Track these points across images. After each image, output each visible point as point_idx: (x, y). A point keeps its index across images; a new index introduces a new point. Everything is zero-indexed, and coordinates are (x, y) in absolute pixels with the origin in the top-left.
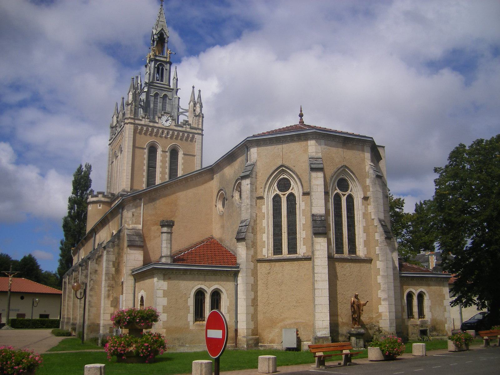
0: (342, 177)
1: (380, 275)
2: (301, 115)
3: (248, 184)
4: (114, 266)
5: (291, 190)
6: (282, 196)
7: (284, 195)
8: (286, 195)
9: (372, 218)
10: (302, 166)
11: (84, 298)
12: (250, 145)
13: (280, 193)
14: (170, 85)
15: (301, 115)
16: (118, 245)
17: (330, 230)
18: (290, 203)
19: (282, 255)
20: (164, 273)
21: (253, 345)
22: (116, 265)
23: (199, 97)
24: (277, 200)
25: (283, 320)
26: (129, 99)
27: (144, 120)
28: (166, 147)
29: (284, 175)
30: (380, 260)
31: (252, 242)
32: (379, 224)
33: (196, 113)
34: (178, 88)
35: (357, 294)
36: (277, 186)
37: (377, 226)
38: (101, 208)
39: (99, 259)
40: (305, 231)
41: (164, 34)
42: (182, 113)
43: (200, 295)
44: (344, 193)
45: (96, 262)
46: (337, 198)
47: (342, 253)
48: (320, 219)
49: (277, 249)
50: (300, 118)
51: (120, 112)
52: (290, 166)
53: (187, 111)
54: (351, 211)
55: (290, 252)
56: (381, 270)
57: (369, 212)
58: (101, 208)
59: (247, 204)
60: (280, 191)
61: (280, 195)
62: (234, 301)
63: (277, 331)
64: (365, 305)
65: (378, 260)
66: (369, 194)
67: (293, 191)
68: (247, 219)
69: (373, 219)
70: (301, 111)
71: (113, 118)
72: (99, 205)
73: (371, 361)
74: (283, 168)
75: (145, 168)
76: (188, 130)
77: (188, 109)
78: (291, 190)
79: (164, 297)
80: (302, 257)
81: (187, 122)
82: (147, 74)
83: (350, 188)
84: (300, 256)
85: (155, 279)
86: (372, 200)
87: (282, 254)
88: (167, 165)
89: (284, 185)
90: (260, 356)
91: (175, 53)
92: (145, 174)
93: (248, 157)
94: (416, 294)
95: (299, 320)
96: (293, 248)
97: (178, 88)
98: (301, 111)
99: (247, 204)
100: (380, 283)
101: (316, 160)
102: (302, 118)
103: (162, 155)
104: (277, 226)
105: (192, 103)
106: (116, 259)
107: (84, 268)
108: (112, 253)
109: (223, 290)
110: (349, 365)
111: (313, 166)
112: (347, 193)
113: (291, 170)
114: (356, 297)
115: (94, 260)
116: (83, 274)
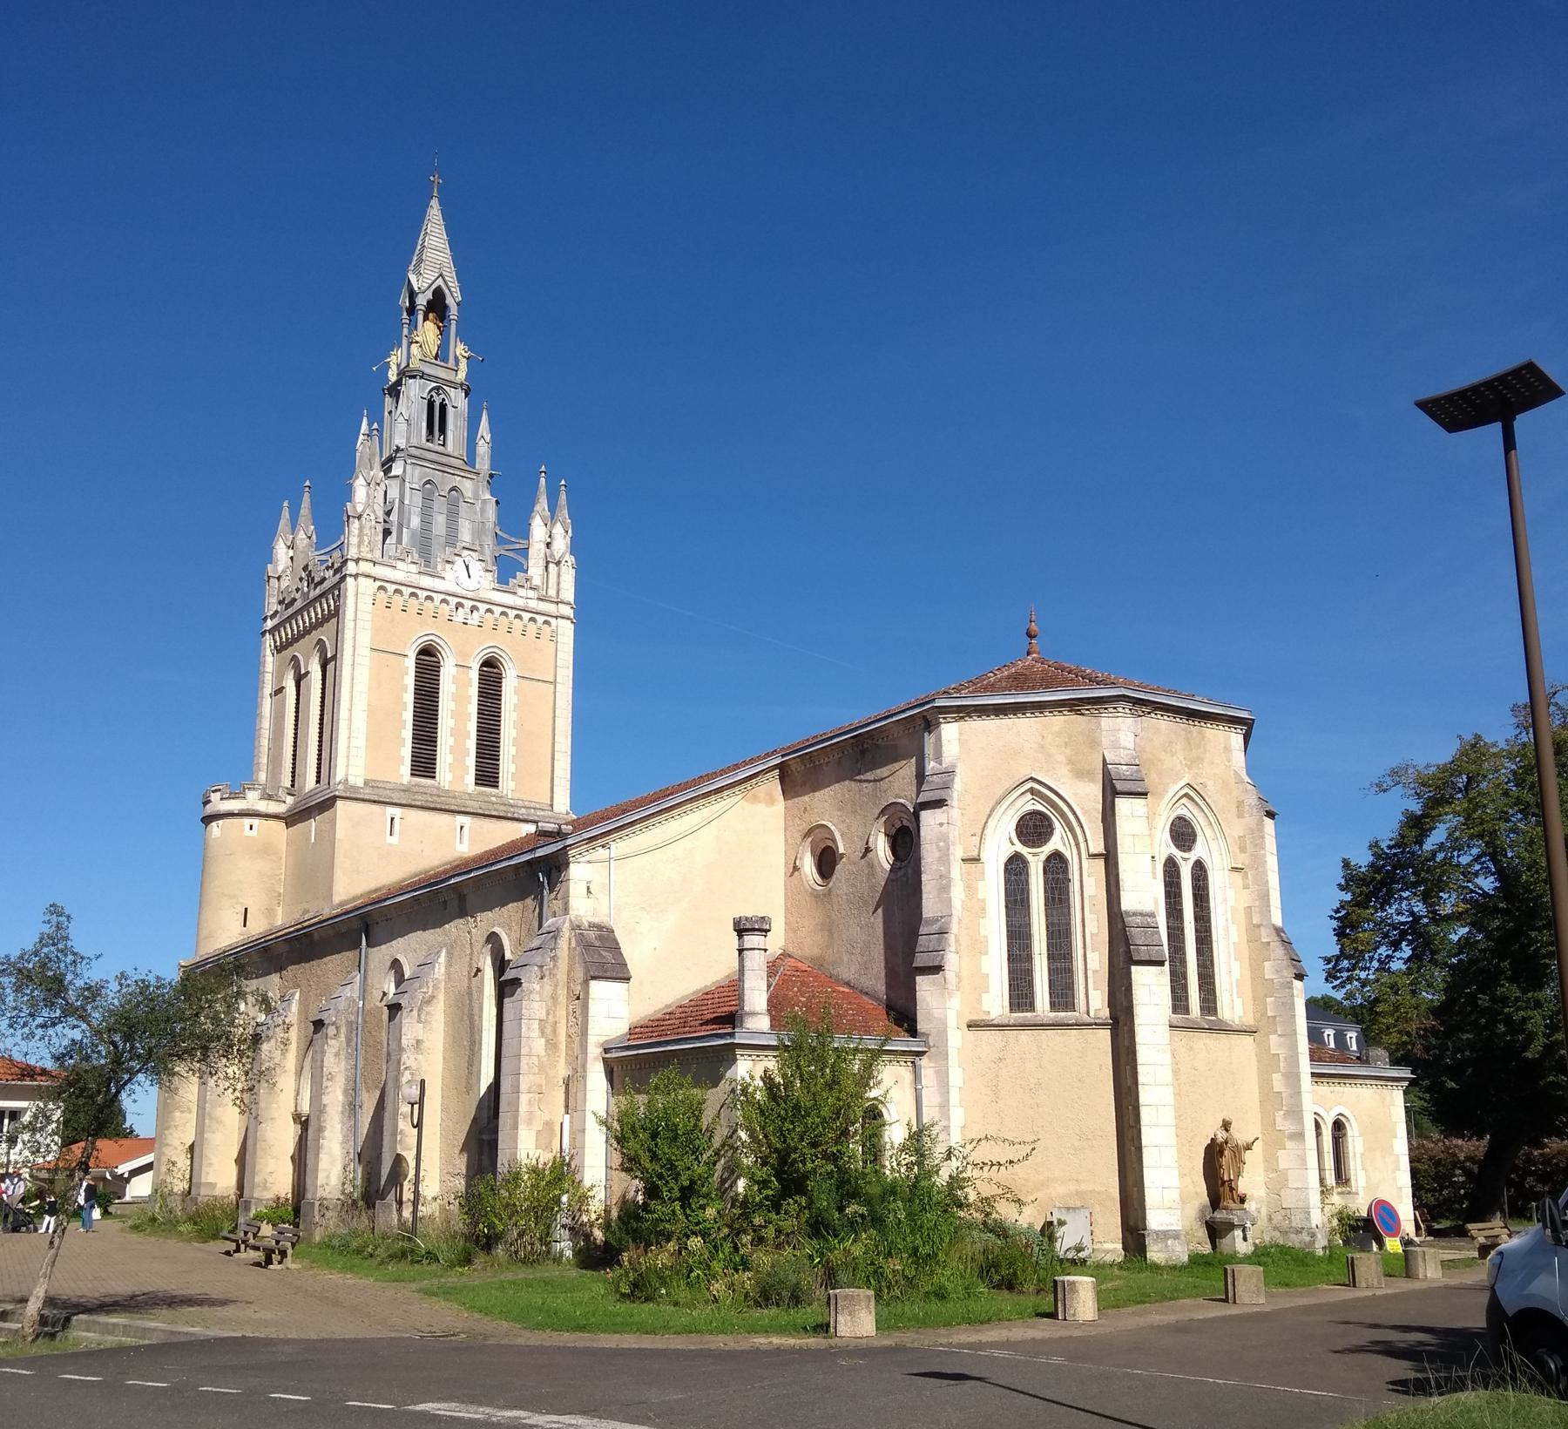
1: (1279, 1072)
4: (542, 1033)
6: (1030, 858)
8: (1043, 857)
13: (1025, 851)
18: (1053, 879)
19: (1035, 1014)
22: (548, 1030)
24: (1015, 868)
28: (465, 655)
30: (1279, 1033)
31: (957, 976)
32: (1276, 939)
33: (555, 553)
37: (1268, 943)
39: (427, 1009)
41: (447, 291)
44: (1186, 855)
45: (419, 1015)
47: (1187, 1010)
49: (1021, 994)
54: (1201, 902)
55: (1054, 1006)
56: (1282, 1059)
60: (1024, 843)
65: (1275, 1032)
68: (942, 917)
76: (533, 604)
91: (483, 360)
100: (1281, 1093)
103: (455, 680)
104: (1018, 936)
106: (548, 1014)
112: (1193, 856)
114: (1226, 1126)
115: (411, 1011)
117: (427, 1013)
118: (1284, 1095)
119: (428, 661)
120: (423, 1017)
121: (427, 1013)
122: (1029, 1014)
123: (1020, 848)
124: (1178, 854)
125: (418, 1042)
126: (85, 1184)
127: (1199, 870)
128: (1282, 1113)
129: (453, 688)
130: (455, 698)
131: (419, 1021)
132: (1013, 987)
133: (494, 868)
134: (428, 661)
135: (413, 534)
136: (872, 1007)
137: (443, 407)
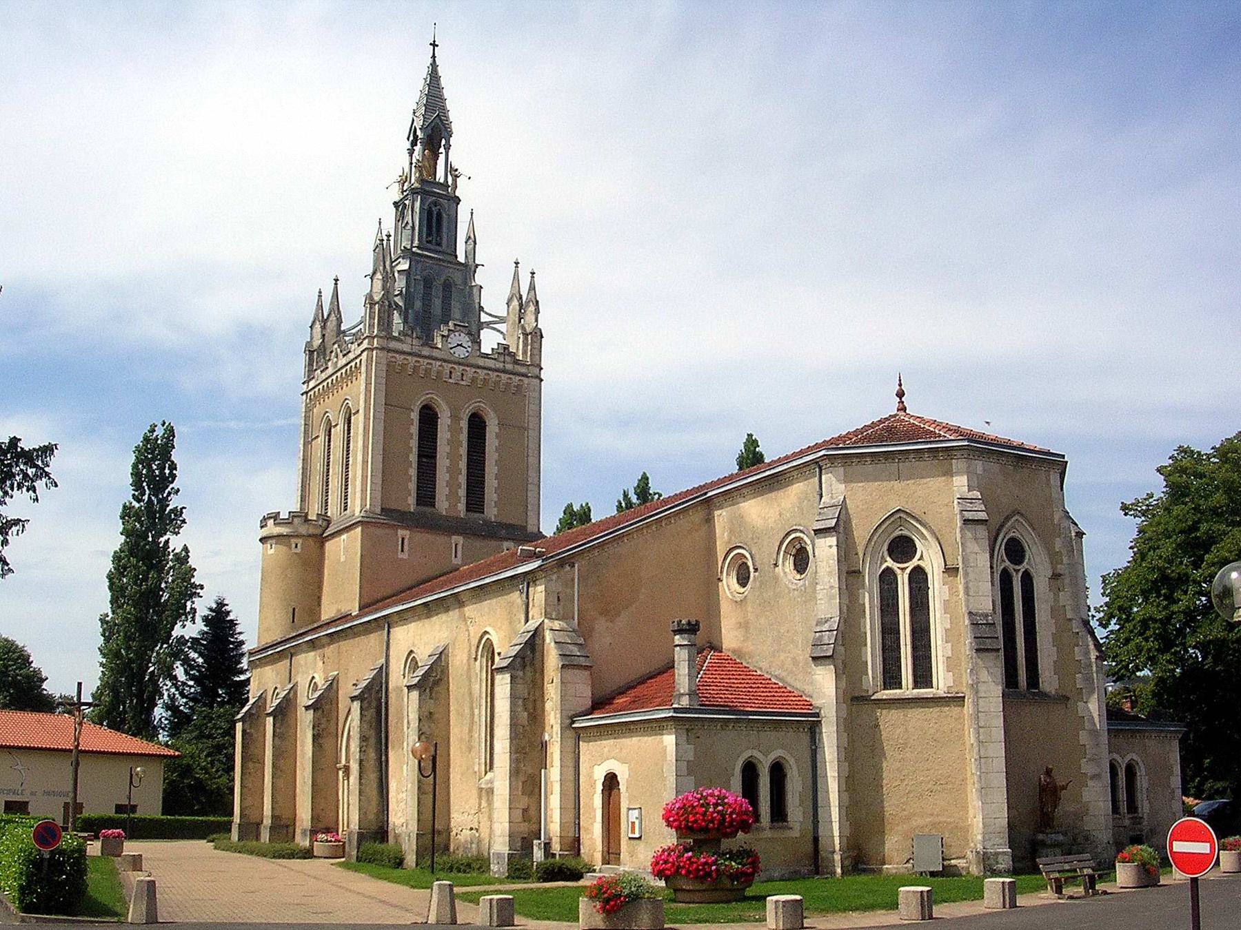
0: (1014, 534)
2: (901, 394)
3: (830, 547)
5: (919, 560)
6: (899, 572)
7: (903, 569)
8: (908, 571)
9: (1068, 617)
10: (941, 513)
11: (432, 776)
12: (828, 465)
14: (458, 253)
15: (901, 394)
16: (532, 664)
17: (864, 617)
19: (902, 691)
20: (687, 727)
21: (850, 868)
22: (530, 706)
23: (532, 288)
25: (908, 818)
26: (374, 290)
27: (409, 340)
29: (901, 530)
34: (477, 262)
35: (1050, 767)
36: (888, 550)
38: (272, 551)
40: (950, 644)
42: (488, 324)
43: (750, 771)
44: (1017, 567)
46: (1006, 579)
48: (985, 622)
49: (891, 678)
50: (898, 400)
51: (329, 315)
52: (916, 512)
53: (502, 320)
55: (917, 685)
57: (1061, 604)
58: (272, 551)
59: (831, 587)
61: (896, 569)
62: (809, 783)
63: (896, 839)
64: (1064, 788)
66: (1060, 568)
67: (921, 563)
69: (1070, 620)
70: (900, 385)
71: (311, 327)
72: (269, 546)
73: (1225, 872)
74: (902, 515)
75: (413, 458)
77: (505, 315)
78: (919, 560)
79: (689, 774)
80: (945, 695)
81: (506, 348)
82: (409, 227)
83: (1027, 557)
84: (941, 693)
85: (665, 737)
86: (1067, 581)
87: (901, 688)
88: (463, 450)
89: (902, 548)
90: (902, 889)
92: (413, 472)
93: (823, 489)
94: (1124, 766)
95: (942, 819)
96: (923, 676)
97: (477, 262)
98: (900, 385)
99: (831, 587)
100: (1085, 745)
101: (971, 503)
102: (903, 399)
104: (890, 631)
105: (515, 303)
107: (367, 705)
108: (521, 681)
109: (792, 761)
110: (1094, 895)
111: (969, 515)
112: (1022, 568)
113: (918, 521)
114: (1048, 772)
115: (425, 690)
116: (364, 719)
117: (437, 692)
118: (1087, 747)
119: (428, 418)
120: (433, 695)
121: (437, 692)
122: (898, 691)
123: (890, 563)
124: (1011, 567)
125: (431, 713)
126: (167, 465)
127: (1027, 579)
128: (1085, 760)
129: (448, 435)
130: (449, 442)
131: (431, 698)
132: (885, 671)
133: (65, 917)
134: (428, 418)
135: (417, 314)
136: (476, 769)
137: (439, 215)
